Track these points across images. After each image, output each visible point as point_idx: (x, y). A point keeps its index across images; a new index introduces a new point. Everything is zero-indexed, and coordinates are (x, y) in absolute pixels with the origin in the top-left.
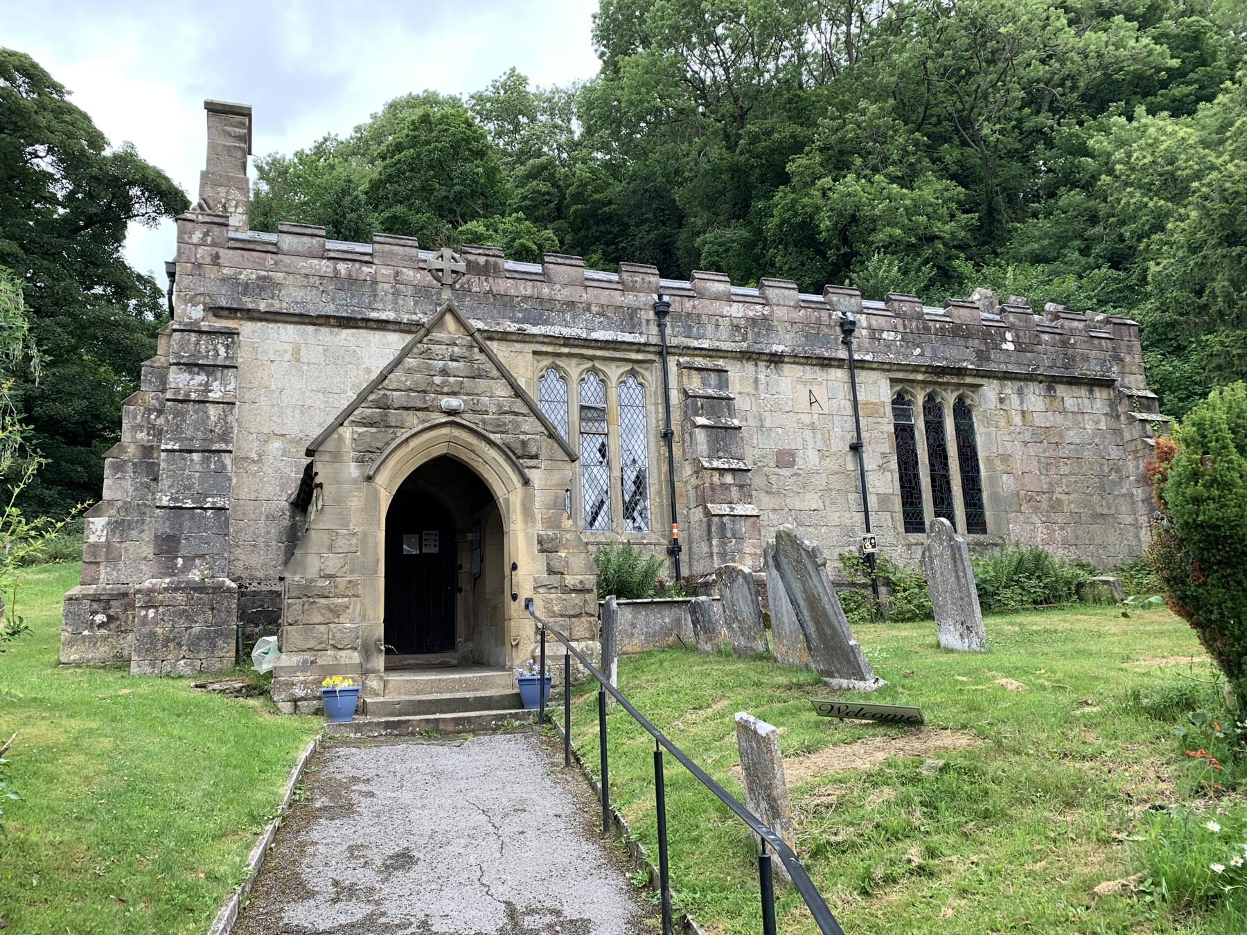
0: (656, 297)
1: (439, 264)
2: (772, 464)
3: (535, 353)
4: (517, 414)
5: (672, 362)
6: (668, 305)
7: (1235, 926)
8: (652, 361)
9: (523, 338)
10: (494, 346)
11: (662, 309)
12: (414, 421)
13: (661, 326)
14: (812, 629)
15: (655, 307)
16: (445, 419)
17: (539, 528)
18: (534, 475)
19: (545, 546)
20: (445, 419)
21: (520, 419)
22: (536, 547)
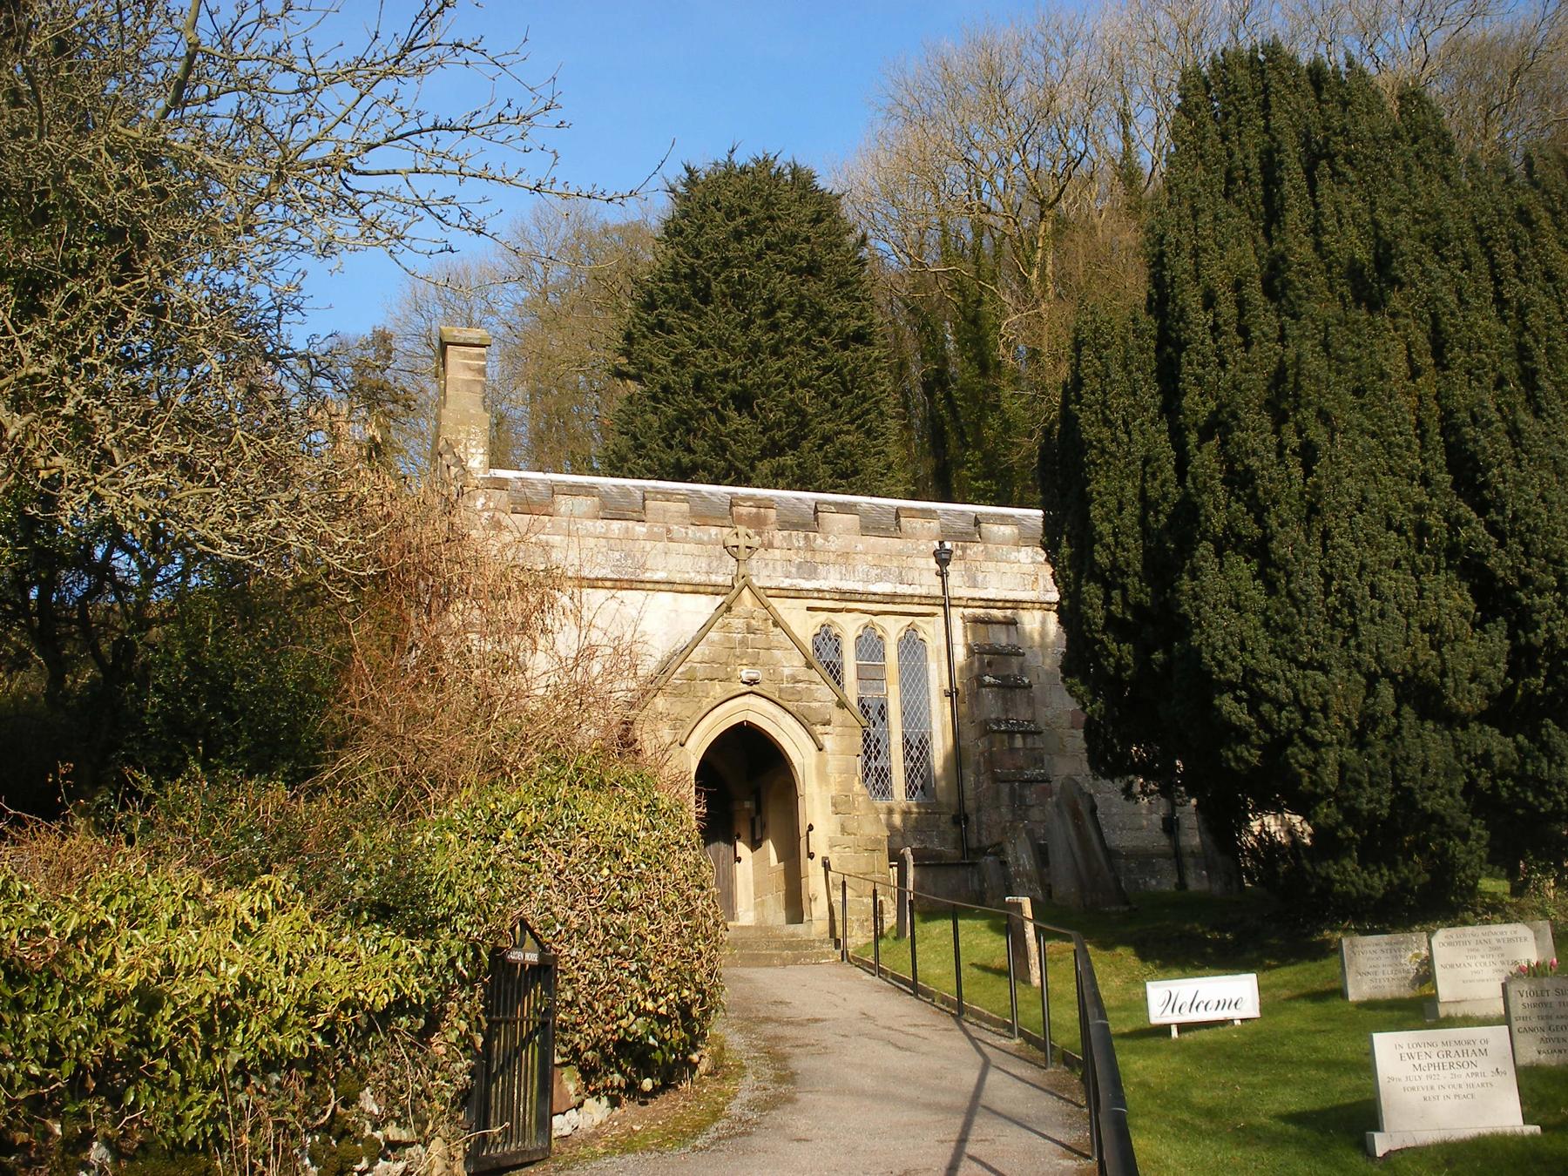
0: (937, 544)
1: (732, 541)
2: (1066, 724)
3: (809, 609)
4: (811, 682)
5: (956, 613)
6: (950, 552)
7: (412, 1059)
8: (933, 615)
9: (798, 594)
10: (775, 602)
11: (944, 556)
12: (718, 690)
13: (943, 575)
14: (1078, 854)
15: (935, 554)
16: (746, 688)
17: (834, 790)
18: (828, 742)
19: (839, 809)
20: (746, 688)
21: (813, 686)
22: (830, 809)
